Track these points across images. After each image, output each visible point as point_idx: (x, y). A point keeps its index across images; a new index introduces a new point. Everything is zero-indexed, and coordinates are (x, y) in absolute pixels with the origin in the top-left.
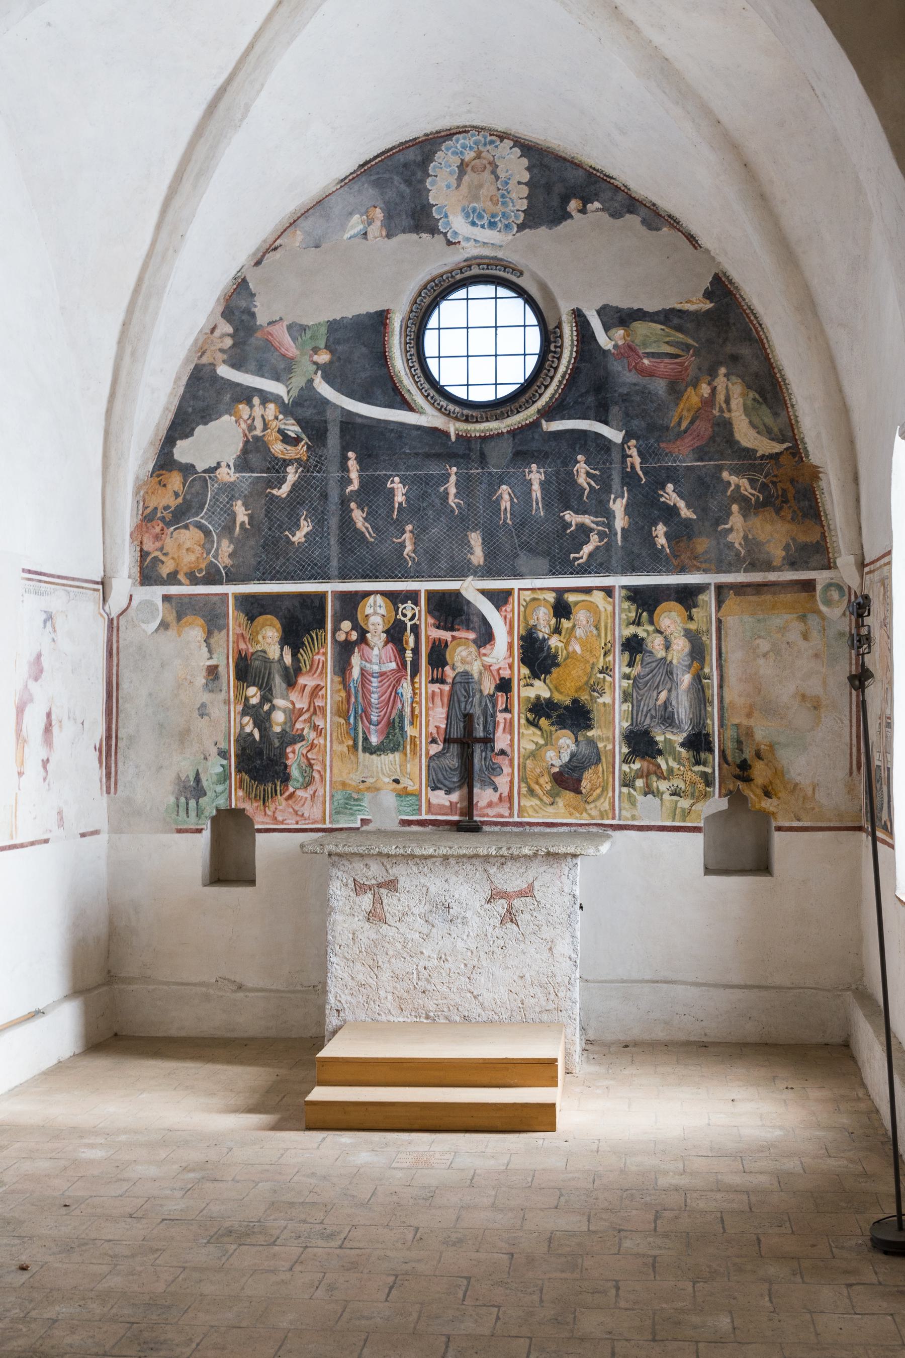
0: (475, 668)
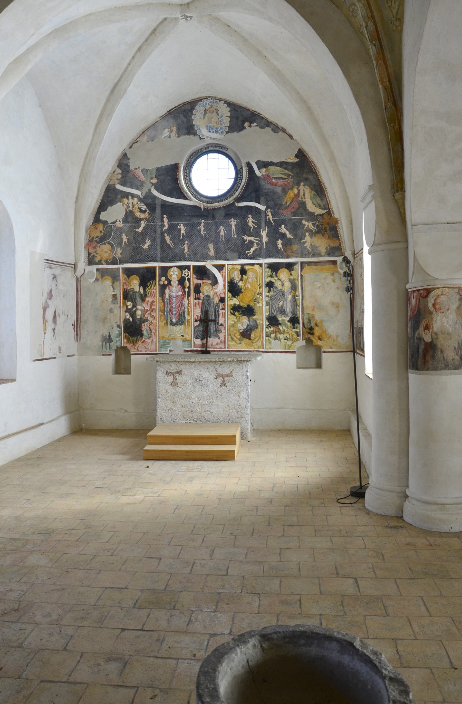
0: (211, 294)
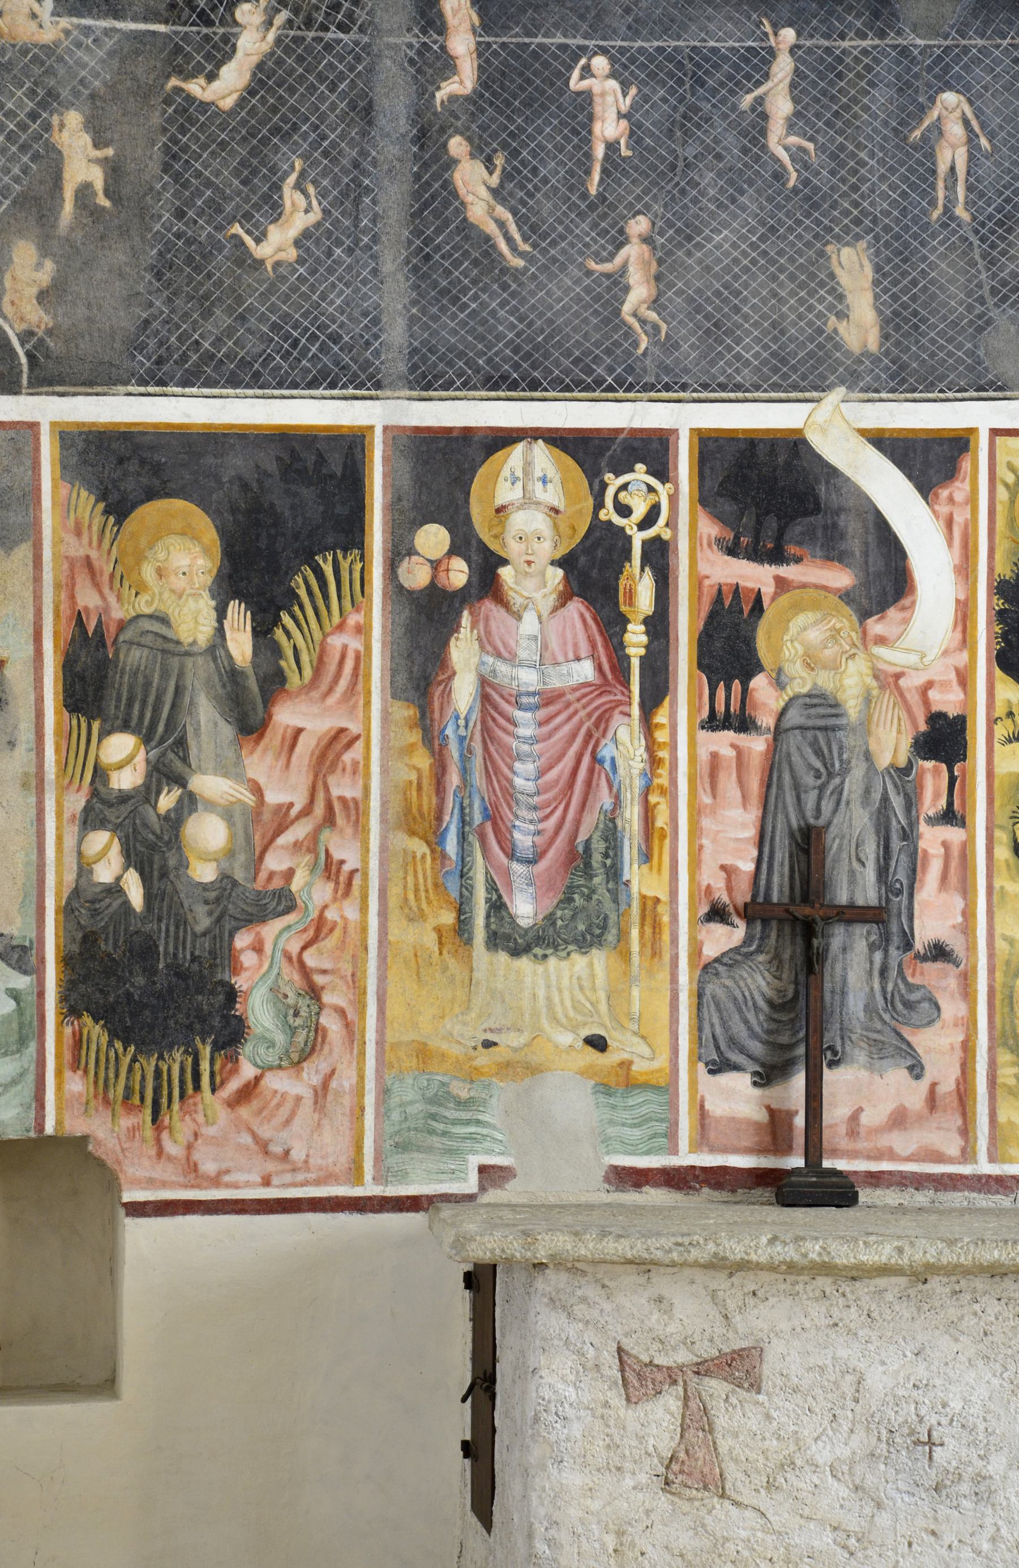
0: (851, 684)
